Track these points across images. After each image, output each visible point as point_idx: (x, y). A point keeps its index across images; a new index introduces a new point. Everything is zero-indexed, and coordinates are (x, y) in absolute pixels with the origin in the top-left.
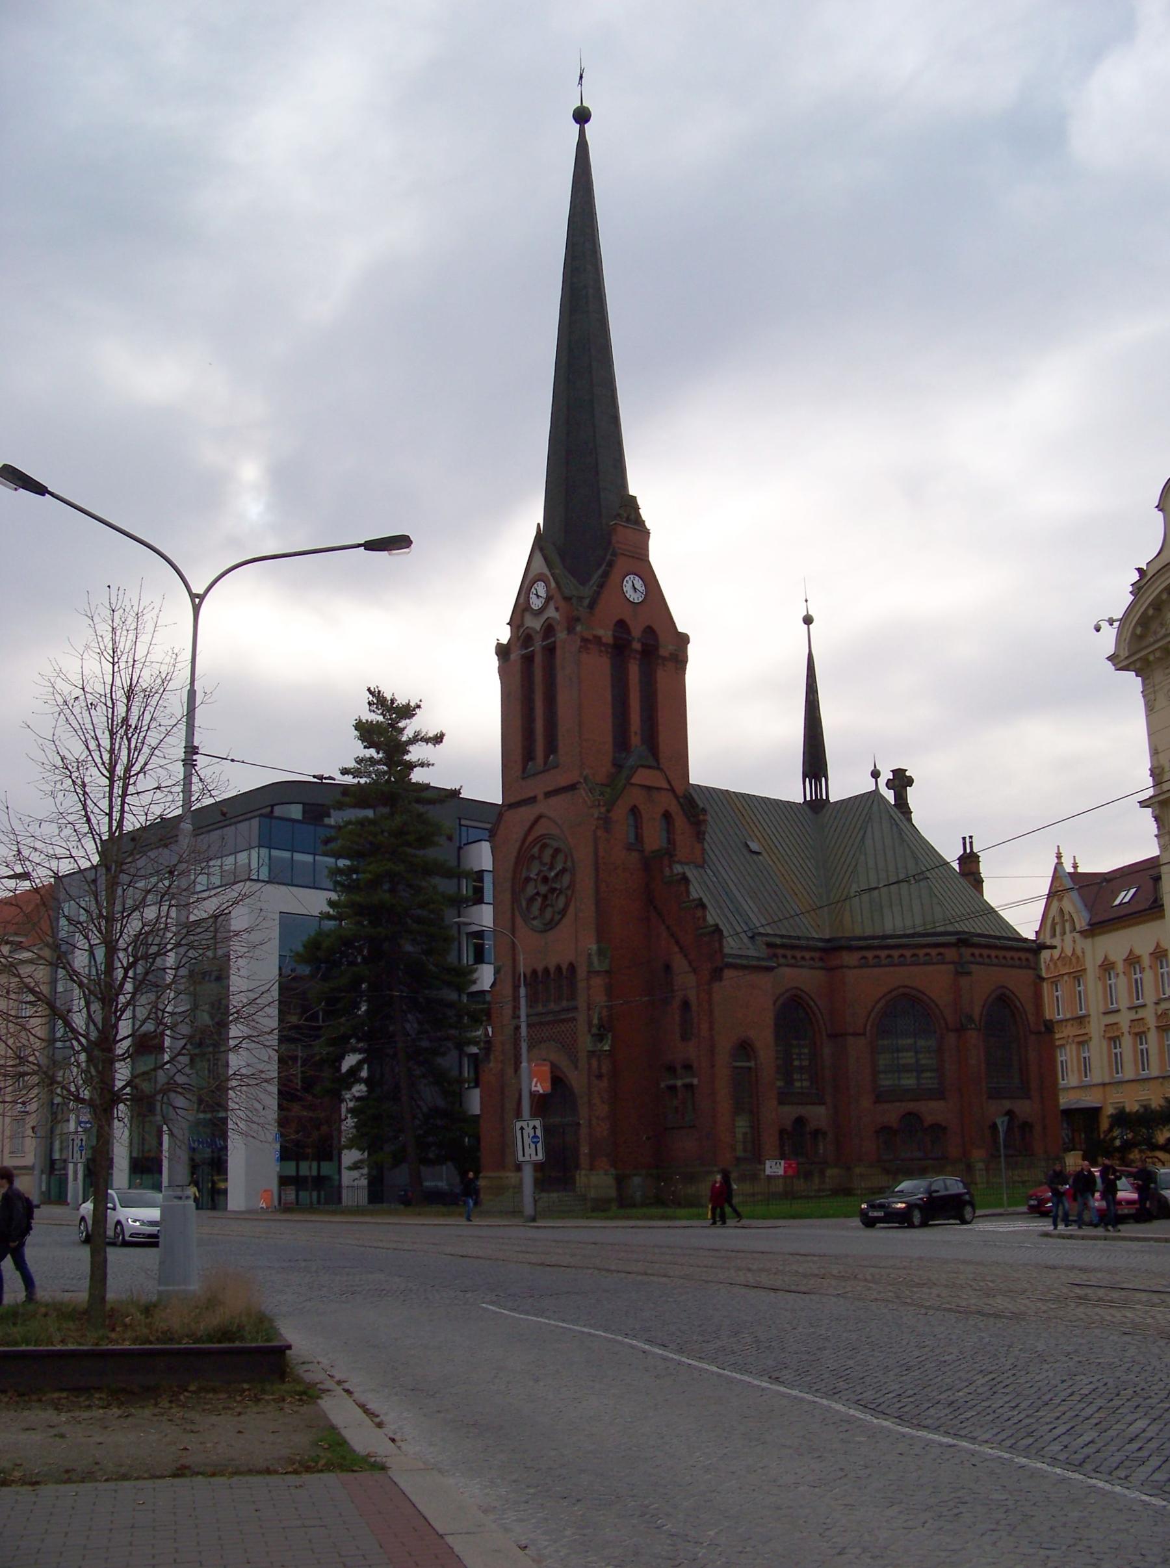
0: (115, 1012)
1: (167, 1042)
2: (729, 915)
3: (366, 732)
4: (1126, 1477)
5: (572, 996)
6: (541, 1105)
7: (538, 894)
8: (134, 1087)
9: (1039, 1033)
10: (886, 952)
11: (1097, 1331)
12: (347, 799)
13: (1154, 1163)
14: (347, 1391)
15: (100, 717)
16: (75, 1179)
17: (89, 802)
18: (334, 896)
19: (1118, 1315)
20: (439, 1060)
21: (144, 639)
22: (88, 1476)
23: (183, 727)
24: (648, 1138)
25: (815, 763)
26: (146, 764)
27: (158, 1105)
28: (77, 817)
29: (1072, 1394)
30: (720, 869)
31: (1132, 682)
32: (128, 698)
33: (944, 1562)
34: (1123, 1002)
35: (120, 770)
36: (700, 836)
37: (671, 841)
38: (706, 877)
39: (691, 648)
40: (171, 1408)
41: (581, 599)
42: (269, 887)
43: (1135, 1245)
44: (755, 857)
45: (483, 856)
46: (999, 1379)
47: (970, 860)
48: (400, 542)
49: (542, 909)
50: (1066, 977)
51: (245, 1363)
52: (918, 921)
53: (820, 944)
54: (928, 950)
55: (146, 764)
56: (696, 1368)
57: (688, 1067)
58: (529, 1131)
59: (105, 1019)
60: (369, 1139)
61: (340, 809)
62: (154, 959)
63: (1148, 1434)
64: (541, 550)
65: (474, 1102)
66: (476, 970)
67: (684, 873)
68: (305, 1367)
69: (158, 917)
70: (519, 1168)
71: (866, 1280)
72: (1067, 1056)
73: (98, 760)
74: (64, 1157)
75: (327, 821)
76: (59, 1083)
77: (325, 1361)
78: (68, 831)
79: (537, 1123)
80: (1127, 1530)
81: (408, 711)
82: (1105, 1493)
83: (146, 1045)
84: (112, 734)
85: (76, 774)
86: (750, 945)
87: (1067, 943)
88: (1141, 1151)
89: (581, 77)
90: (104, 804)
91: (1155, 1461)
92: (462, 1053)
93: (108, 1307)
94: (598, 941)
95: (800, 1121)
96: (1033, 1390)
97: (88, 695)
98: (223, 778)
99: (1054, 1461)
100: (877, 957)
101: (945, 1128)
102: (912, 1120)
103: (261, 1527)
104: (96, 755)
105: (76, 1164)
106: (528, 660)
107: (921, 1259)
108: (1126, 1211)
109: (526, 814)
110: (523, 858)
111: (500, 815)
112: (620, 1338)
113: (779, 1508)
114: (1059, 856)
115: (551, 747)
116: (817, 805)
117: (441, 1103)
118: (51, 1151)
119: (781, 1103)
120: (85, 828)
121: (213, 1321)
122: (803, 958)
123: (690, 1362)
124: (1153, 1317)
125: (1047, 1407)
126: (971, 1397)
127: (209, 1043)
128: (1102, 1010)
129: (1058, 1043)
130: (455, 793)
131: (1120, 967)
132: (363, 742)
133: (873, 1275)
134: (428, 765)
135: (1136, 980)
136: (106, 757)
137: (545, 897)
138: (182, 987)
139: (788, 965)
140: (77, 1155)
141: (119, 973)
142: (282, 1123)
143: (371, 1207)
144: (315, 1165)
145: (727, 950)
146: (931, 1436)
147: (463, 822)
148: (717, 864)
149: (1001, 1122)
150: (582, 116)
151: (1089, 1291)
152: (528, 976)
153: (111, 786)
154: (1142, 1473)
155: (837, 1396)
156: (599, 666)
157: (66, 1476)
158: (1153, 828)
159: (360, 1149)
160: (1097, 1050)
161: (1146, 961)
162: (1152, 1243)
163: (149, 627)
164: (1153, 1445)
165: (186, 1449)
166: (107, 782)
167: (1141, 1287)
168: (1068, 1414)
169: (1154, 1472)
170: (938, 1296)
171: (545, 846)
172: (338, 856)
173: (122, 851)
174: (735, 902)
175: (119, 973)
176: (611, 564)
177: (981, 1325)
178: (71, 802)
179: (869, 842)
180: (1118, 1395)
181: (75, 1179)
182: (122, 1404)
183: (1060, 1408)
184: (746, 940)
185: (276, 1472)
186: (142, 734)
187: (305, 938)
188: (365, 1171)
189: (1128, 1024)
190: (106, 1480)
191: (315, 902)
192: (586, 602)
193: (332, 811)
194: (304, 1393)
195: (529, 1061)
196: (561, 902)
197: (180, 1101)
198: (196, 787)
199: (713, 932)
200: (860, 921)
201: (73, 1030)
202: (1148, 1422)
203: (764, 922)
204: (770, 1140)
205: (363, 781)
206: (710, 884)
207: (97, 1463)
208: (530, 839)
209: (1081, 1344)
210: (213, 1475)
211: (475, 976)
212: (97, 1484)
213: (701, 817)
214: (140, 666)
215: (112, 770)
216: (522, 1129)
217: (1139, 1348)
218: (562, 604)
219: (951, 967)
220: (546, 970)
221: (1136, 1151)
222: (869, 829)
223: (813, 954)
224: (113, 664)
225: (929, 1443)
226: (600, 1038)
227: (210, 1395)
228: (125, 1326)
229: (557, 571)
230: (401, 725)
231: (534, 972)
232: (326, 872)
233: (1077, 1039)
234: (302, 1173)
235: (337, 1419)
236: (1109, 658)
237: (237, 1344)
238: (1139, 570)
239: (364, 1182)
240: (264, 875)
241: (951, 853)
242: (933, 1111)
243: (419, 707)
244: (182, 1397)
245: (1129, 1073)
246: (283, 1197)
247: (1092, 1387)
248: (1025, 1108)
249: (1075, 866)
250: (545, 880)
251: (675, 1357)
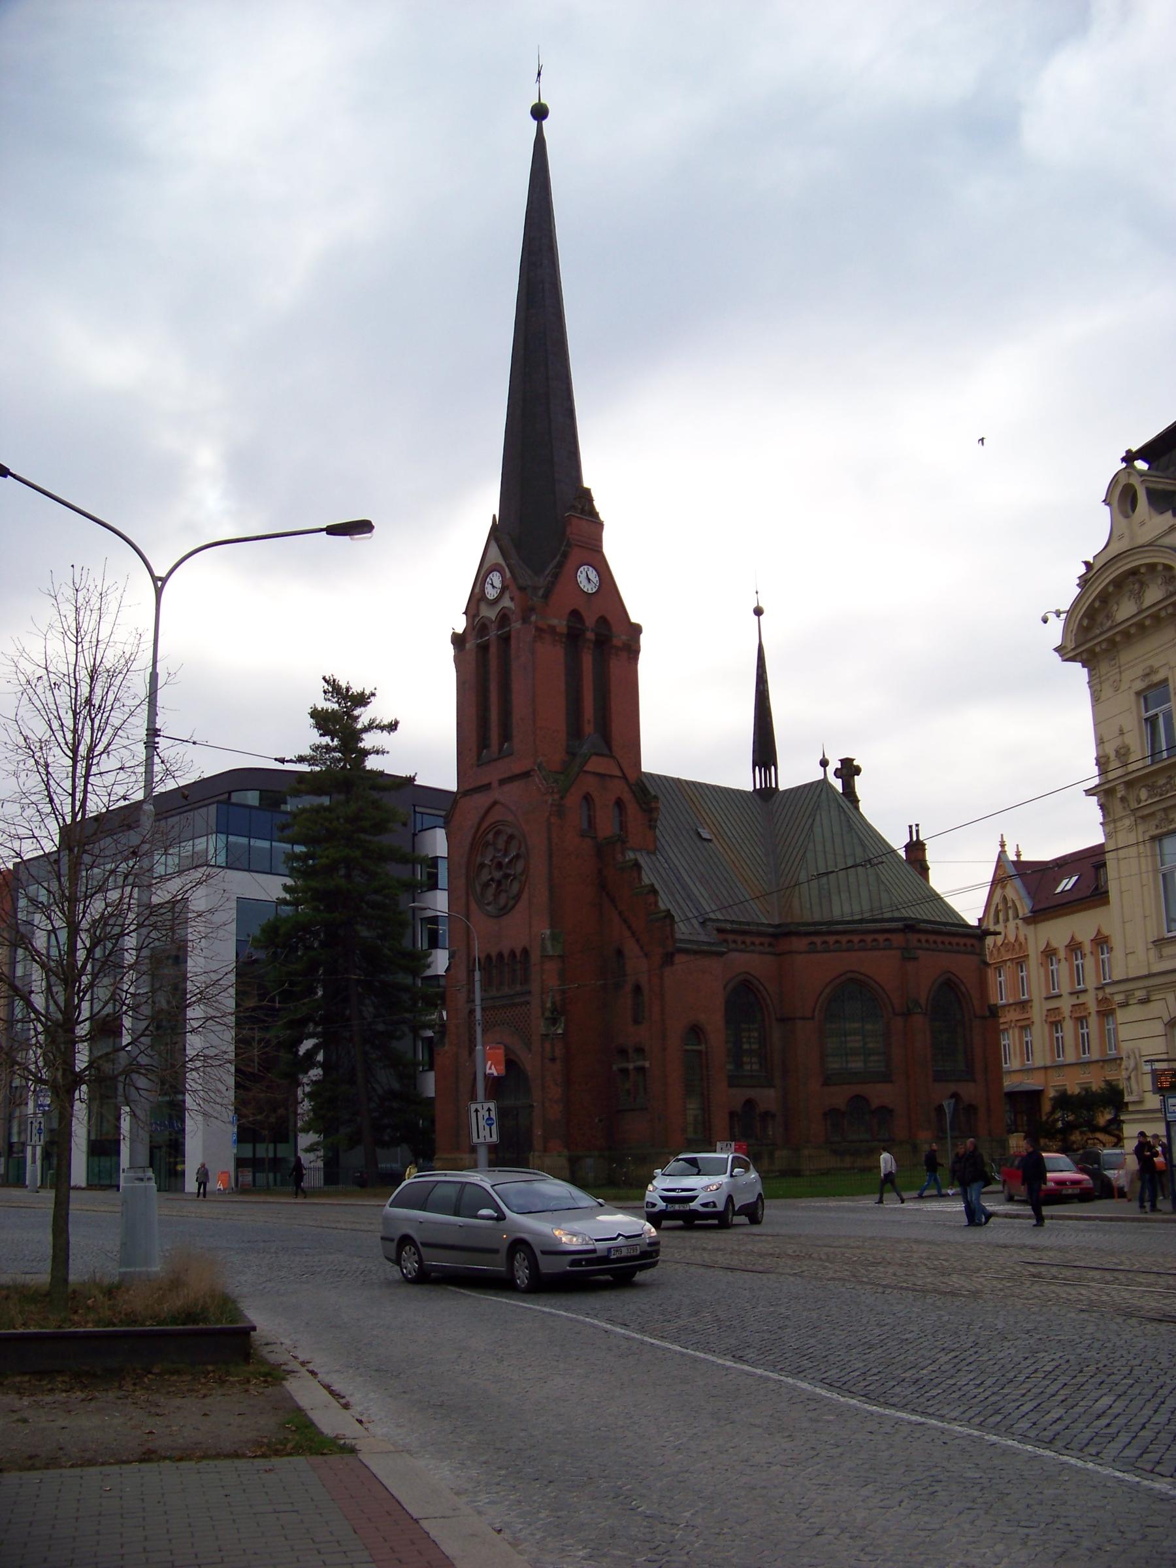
0: (78, 994)
1: (127, 1022)
2: (681, 901)
3: (322, 720)
4: (1098, 1454)
5: (526, 980)
6: (495, 1087)
7: (492, 879)
8: (98, 1069)
9: (984, 1018)
10: (834, 938)
11: (1054, 1309)
12: (303, 787)
13: (1094, 1144)
14: (312, 1373)
15: (63, 697)
16: (34, 1162)
17: (52, 782)
18: (289, 882)
19: (1073, 1292)
20: (395, 1044)
21: (107, 621)
22: (52, 1463)
23: (145, 707)
24: (600, 1121)
25: (764, 752)
26: (109, 744)
27: (120, 1086)
28: (40, 798)
29: (1036, 1371)
30: (671, 855)
31: (1078, 673)
32: (92, 678)
33: (923, 1542)
34: (1065, 987)
35: (83, 750)
36: (652, 825)
37: (623, 826)
38: (657, 864)
39: (643, 639)
40: (134, 1391)
41: (536, 589)
42: (230, 873)
43: (1082, 1224)
44: (706, 844)
45: (438, 843)
46: (962, 1357)
47: (916, 848)
48: (361, 527)
49: (497, 895)
50: (1009, 963)
51: (210, 1344)
52: (866, 907)
53: (771, 930)
55: (109, 744)
56: (658, 1347)
57: (640, 1051)
58: (483, 1113)
59: (69, 1000)
60: (324, 1122)
61: (296, 796)
62: (117, 940)
63: (1114, 1411)
64: (497, 540)
65: (429, 1085)
66: (430, 955)
67: (636, 860)
68: (269, 1348)
69: (121, 898)
70: (473, 1149)
71: (821, 1259)
72: (1010, 1040)
73: (61, 740)
74: (22, 1139)
75: (283, 807)
76: (19, 1064)
77: (287, 1341)
78: (30, 812)
79: (492, 1105)
80: (1103, 1507)
81: (362, 700)
82: (1079, 1470)
83: (106, 1028)
84: (75, 714)
85: (39, 754)
86: (700, 930)
87: (1011, 930)
88: (1082, 1133)
89: (539, 74)
90: (67, 785)
91: (1124, 1438)
92: (416, 1036)
93: (70, 1289)
94: (552, 927)
95: (750, 1103)
96: (997, 1367)
97: (51, 675)
98: (187, 758)
99: (1024, 1438)
100: (824, 942)
101: (891, 1111)
102: (859, 1102)
103: (232, 1513)
104: (59, 735)
105: (34, 1147)
106: (483, 649)
107: (872, 1238)
108: (1070, 1191)
109: (481, 801)
110: (478, 843)
111: (455, 802)
112: (581, 1318)
113: (754, 1489)
114: (1003, 845)
115: (506, 736)
116: (767, 794)
117: (396, 1086)
118: (10, 1134)
119: (731, 1085)
120: (48, 809)
121: (177, 1302)
122: (753, 943)
123: (653, 1341)
124: (1108, 1295)
125: (1012, 1385)
126: (934, 1375)
127: (168, 1025)
128: (1044, 995)
129: (1002, 1027)
130: (411, 779)
131: (1062, 954)
132: (319, 729)
133: (827, 1254)
134: (383, 753)
135: (1077, 966)
136: (69, 736)
137: (499, 883)
138: (144, 968)
139: (737, 950)
140: (35, 1138)
141: (81, 955)
142: (240, 1105)
143: (326, 1189)
144: (271, 1146)
145: (678, 936)
146: (899, 1414)
147: (418, 809)
148: (667, 847)
149: (948, 1105)
150: (540, 113)
151: (1042, 1269)
152: (482, 961)
153: (74, 767)
154: (1113, 1448)
155: (802, 1375)
156: (553, 655)
157: (30, 1463)
158: (1098, 816)
159: (316, 1132)
160: (1039, 1034)
161: (1087, 948)
162: (1097, 1222)
163: (113, 607)
164: (1121, 1421)
165: (151, 1432)
166: (70, 762)
167: (1093, 1265)
168: (1033, 1391)
169: (1124, 1448)
170: (895, 1275)
171: (498, 833)
172: (294, 842)
173: (83, 836)
174: (686, 888)
175: (81, 955)
176: (565, 555)
177: (939, 1303)
178: (34, 782)
179: (817, 829)
180: (1081, 1372)
181: (34, 1162)
182: (86, 1387)
183: (1024, 1386)
184: (697, 925)
185: (244, 1456)
186: (106, 714)
187: (265, 922)
188: (321, 1153)
189: (1070, 1008)
190: (72, 1466)
191: (271, 888)
192: (541, 592)
193: (288, 798)
194: (266, 1375)
195: (484, 1045)
196: (516, 886)
197: (142, 1082)
198: (158, 768)
199: (665, 917)
200: (809, 907)
201: (35, 1011)
202: (1113, 1398)
203: (714, 907)
204: (720, 1121)
205: (318, 769)
206: (661, 870)
207: (61, 1449)
209: (1039, 1322)
210: (181, 1459)
211: (430, 960)
212: (64, 1471)
213: (653, 805)
214: (104, 646)
215: (75, 750)
216: (477, 1111)
217: (1098, 1325)
220: (500, 955)
221: (1077, 1133)
222: (818, 817)
223: (762, 939)
224: (77, 644)
225: (899, 1422)
226: (554, 1022)
227: (175, 1378)
228: (88, 1308)
229: (512, 562)
230: (356, 713)
231: (489, 957)
232: (282, 858)
233: (1020, 1024)
234: (258, 1155)
235: (304, 1401)
236: (1056, 650)
237: (201, 1326)
238: (1087, 563)
239: (320, 1164)
240: (221, 860)
241: (898, 841)
242: (881, 1094)
243: (373, 695)
244: (146, 1380)
245: (1070, 1056)
246: (240, 1179)
247: (1054, 1363)
248: (969, 1091)
249: (1018, 855)
250: (500, 866)
251: (638, 1336)
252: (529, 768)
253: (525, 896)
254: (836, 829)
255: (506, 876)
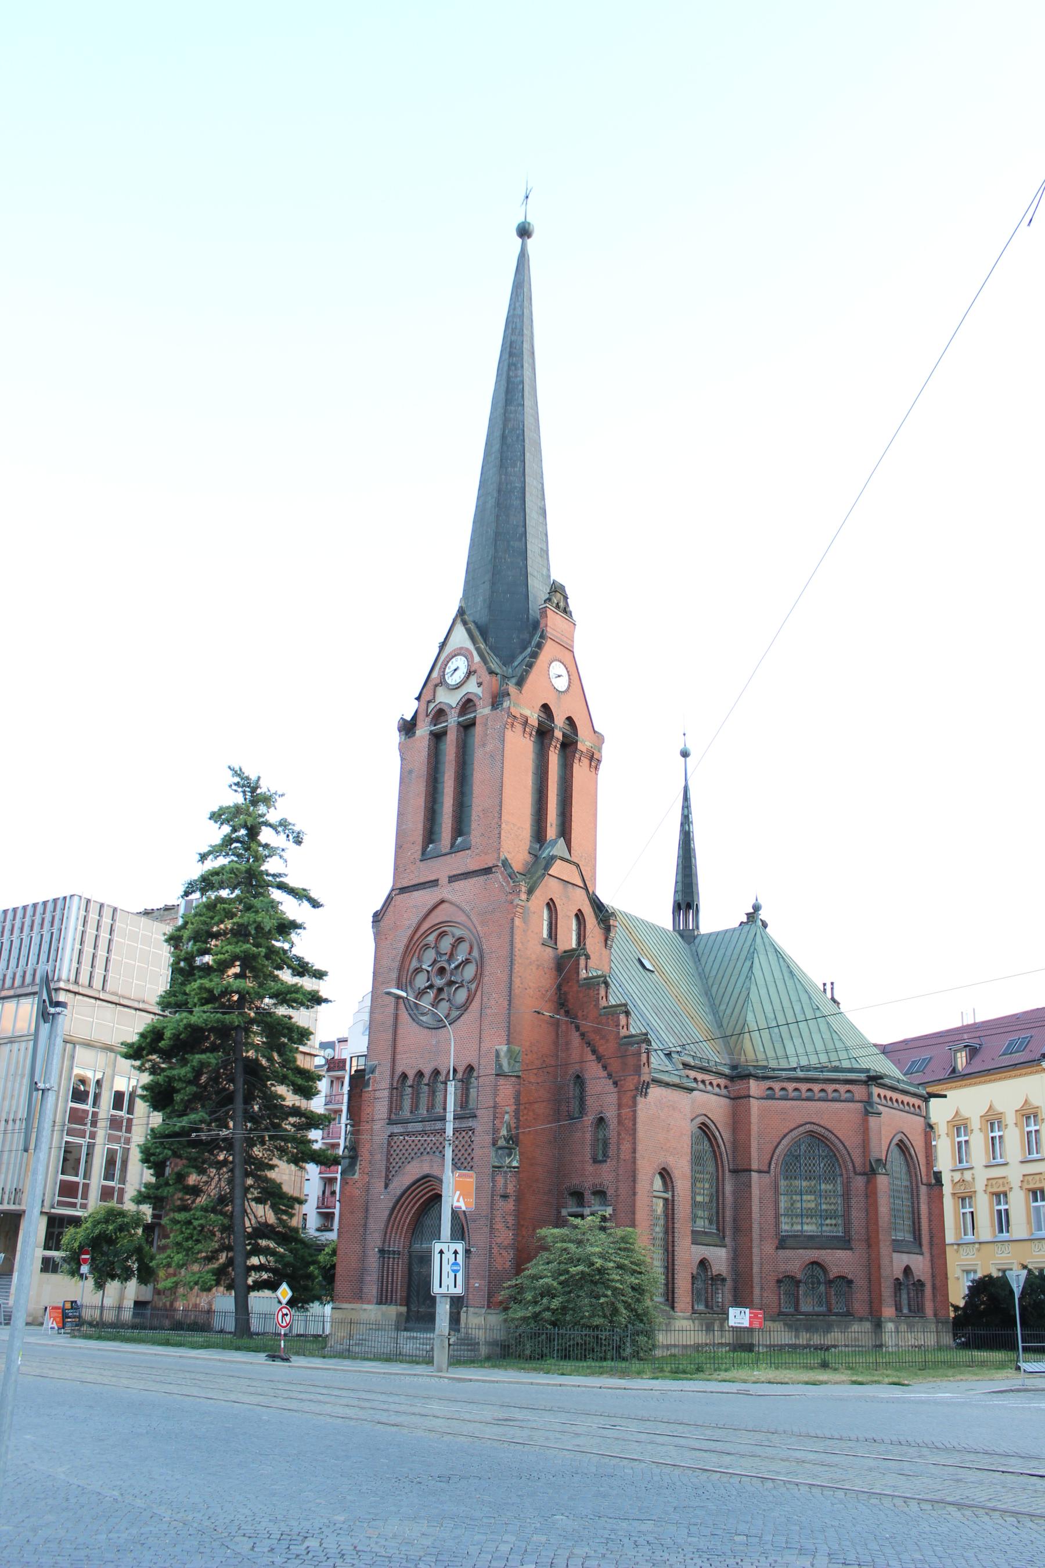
7: (431, 987)
54: (837, 1086)
57: (600, 1194)
58: (448, 1256)
81: (267, 800)
94: (509, 1043)
106: (438, 737)
109: (425, 899)
115: (460, 828)
117: (271, 1218)
171: (443, 934)
176: (539, 646)
184: (663, 1056)
196: (461, 996)
208: (426, 926)
216: (441, 1252)
218: (486, 677)
219: (860, 1106)
222: (756, 960)
250: (442, 971)
252: (491, 865)
253: (475, 1005)
254: (777, 974)
255: (451, 983)
